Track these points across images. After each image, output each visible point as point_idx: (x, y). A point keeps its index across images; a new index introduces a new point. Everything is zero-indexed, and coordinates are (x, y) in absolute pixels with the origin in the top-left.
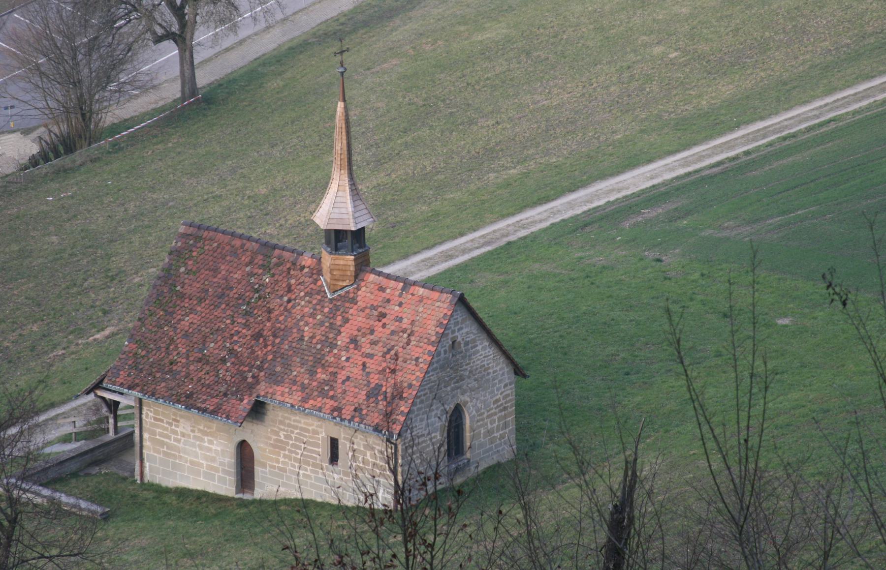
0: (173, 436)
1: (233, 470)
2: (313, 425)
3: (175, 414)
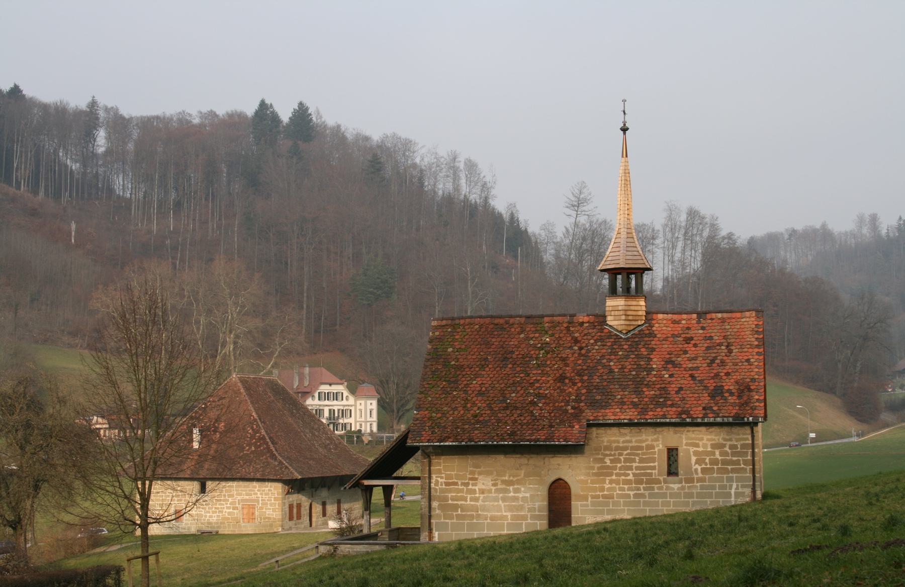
0: (469, 496)
1: (545, 513)
2: (647, 440)
3: (472, 473)
